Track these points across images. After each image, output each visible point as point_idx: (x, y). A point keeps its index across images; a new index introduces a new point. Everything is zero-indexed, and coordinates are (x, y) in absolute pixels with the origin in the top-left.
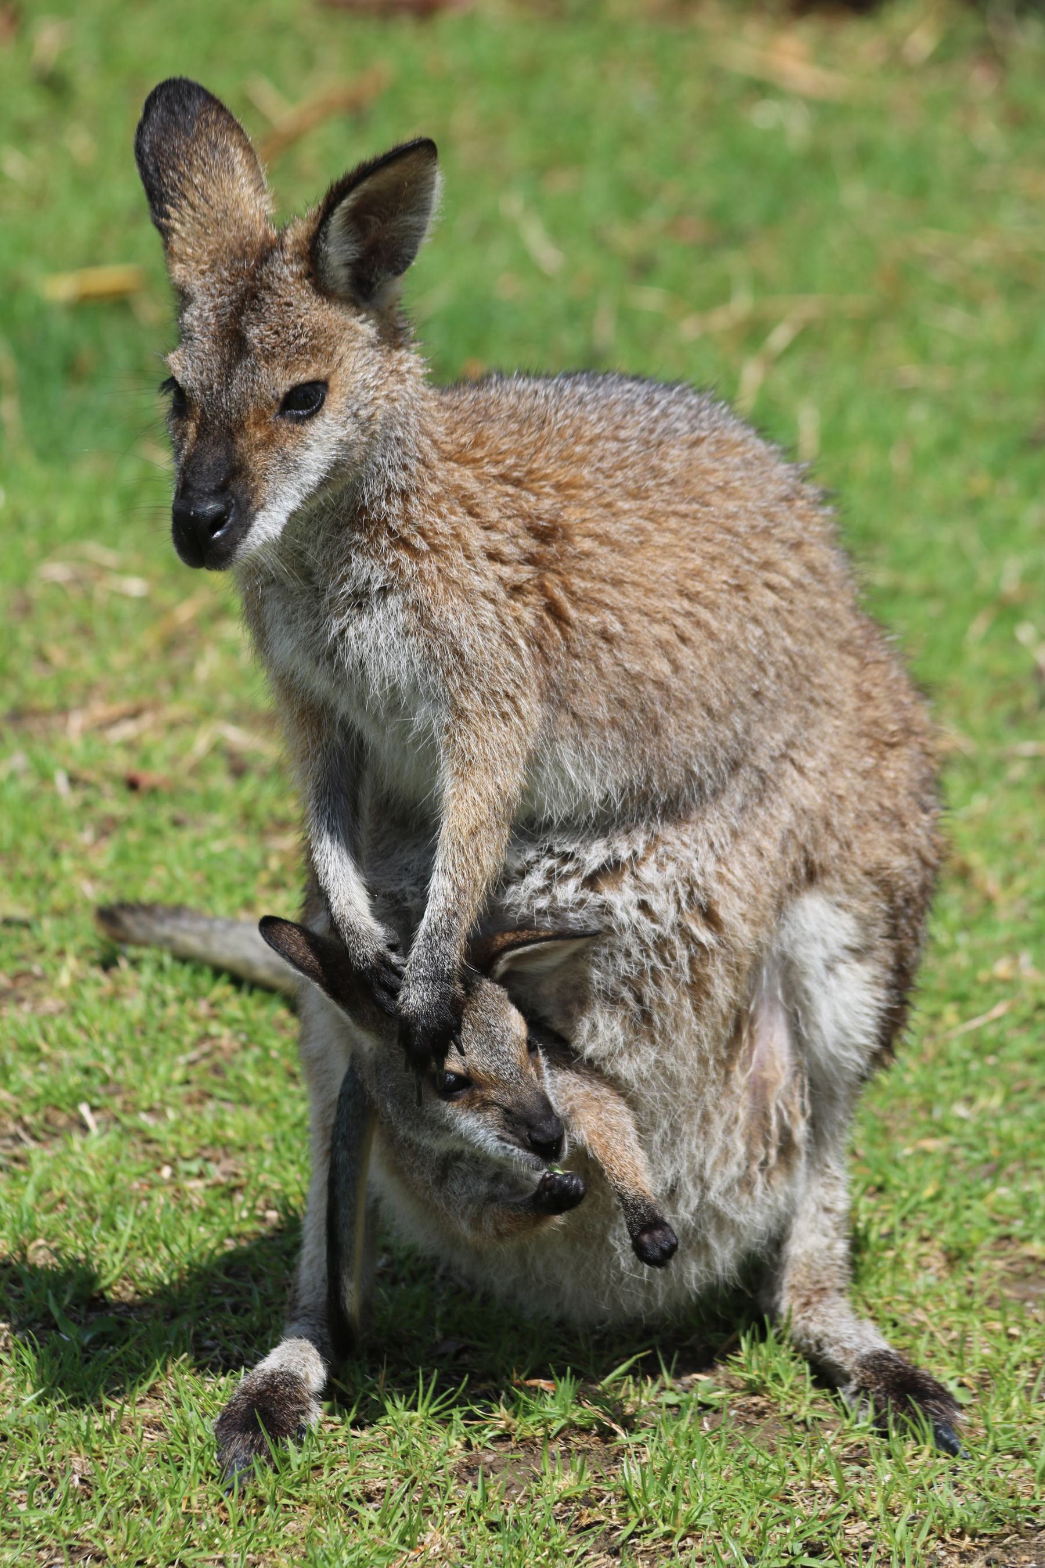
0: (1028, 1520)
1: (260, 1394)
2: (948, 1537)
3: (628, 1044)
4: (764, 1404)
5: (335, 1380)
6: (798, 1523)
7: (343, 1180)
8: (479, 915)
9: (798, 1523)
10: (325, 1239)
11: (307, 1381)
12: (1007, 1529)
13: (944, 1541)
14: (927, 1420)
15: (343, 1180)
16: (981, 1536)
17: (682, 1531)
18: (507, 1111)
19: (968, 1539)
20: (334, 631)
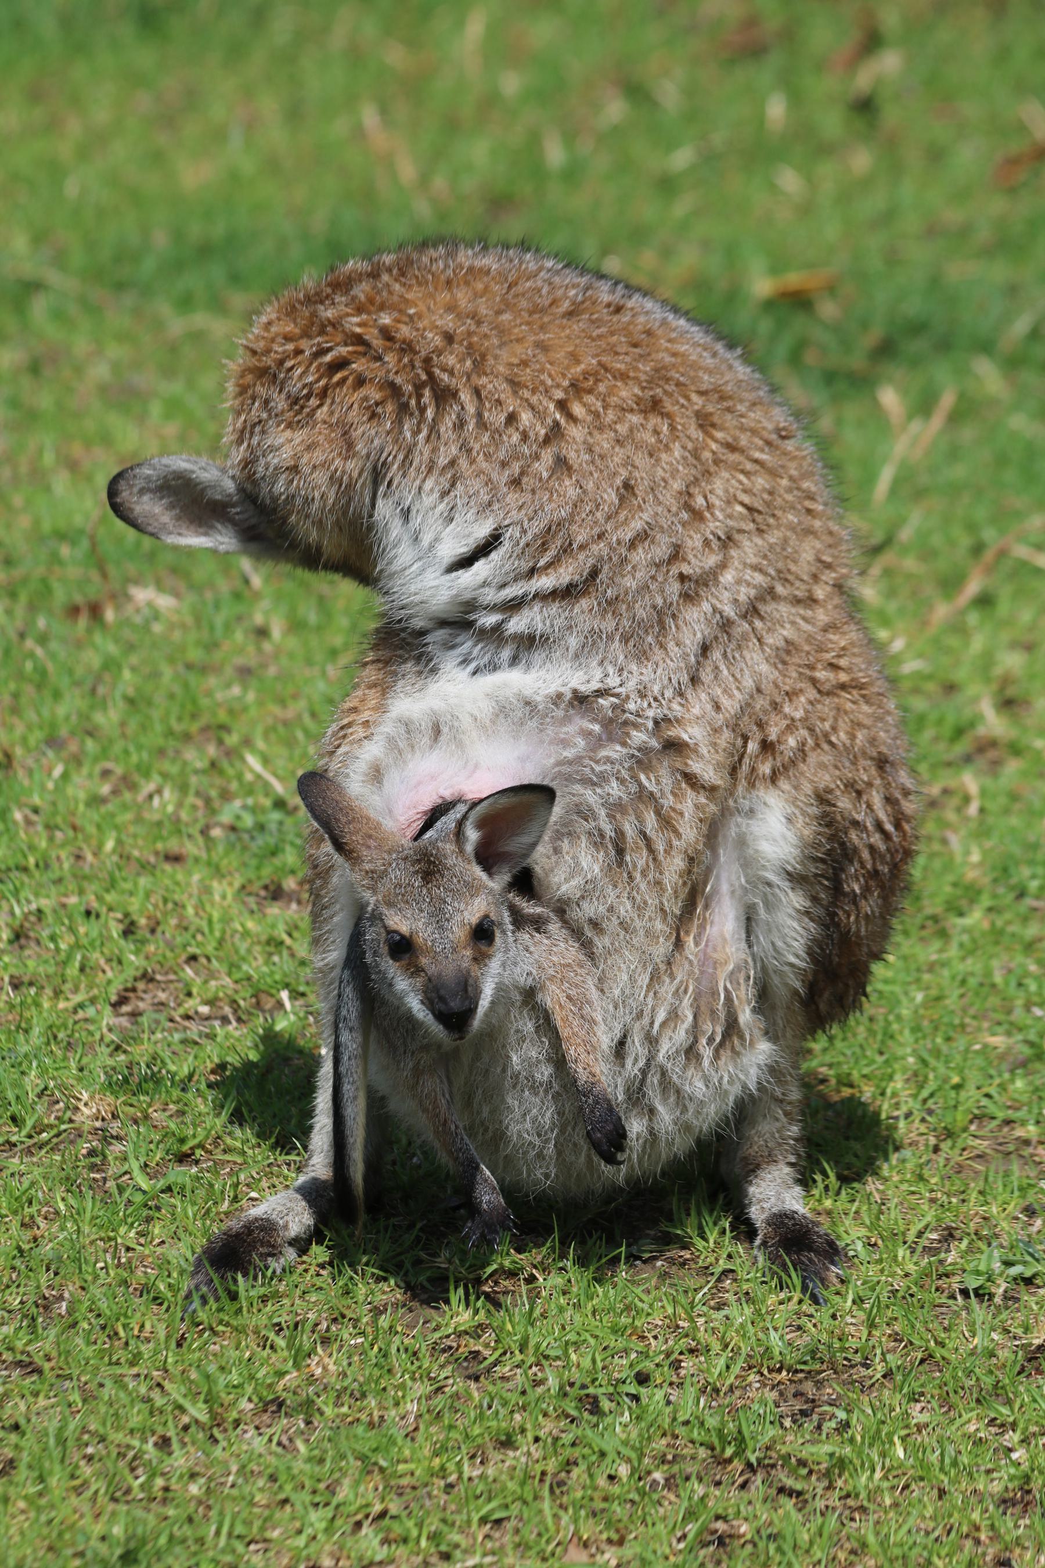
0: (846, 1359)
1: (238, 1235)
2: (766, 1372)
3: (88, 718)
4: (688, 1256)
5: (321, 1227)
6: (633, 1356)
7: (346, 1058)
8: (843, 1023)
9: (633, 1356)
10: (331, 1112)
11: (286, 1227)
12: (825, 1367)
13: (762, 1375)
14: (796, 1270)
15: (346, 1058)
16: (796, 1371)
17: (532, 1359)
18: (430, 980)
19: (784, 1373)
20: (241, 516)
